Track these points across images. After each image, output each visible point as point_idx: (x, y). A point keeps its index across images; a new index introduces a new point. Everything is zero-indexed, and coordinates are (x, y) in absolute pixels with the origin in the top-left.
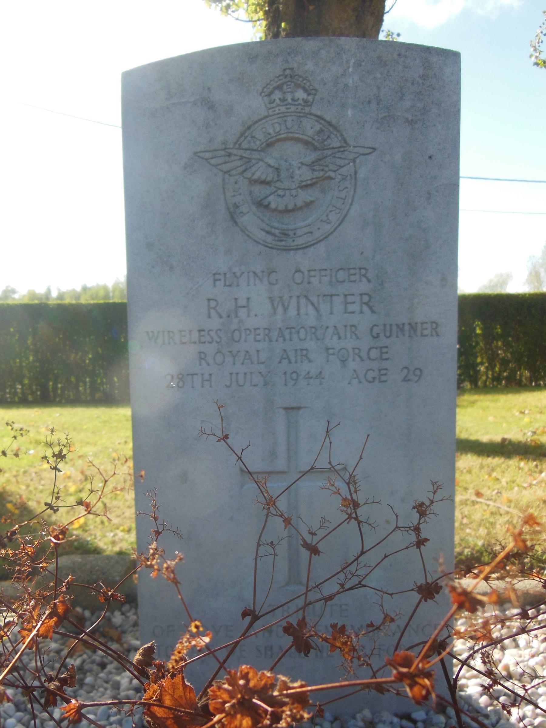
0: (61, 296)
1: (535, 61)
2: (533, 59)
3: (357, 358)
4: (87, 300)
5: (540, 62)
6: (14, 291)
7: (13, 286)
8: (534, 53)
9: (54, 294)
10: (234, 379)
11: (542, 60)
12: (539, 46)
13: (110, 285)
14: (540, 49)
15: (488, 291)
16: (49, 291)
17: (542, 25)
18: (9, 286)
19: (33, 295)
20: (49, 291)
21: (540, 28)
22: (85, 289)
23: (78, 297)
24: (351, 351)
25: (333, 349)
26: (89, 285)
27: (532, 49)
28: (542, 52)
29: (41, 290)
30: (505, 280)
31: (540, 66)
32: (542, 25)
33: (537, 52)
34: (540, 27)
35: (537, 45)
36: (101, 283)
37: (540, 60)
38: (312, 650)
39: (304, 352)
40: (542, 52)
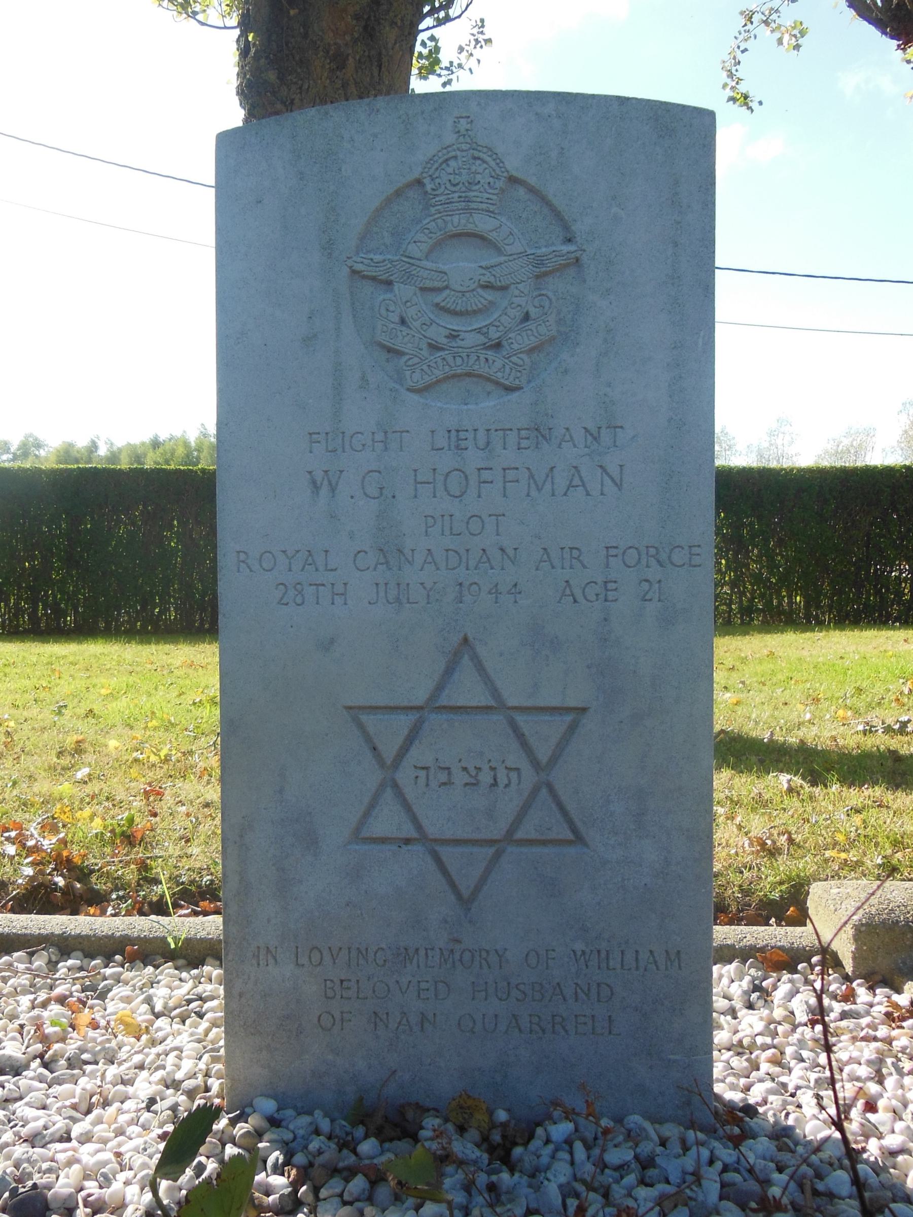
0: (114, 457)
1: (732, 94)
2: (728, 93)
3: (653, 562)
4: (158, 464)
5: (739, 97)
6: (39, 446)
7: (41, 437)
8: (729, 81)
9: (103, 451)
10: (382, 594)
11: (742, 94)
12: (737, 71)
13: (192, 438)
14: (738, 75)
15: (825, 463)
16: (94, 446)
17: (737, 35)
18: (31, 435)
19: (67, 453)
20: (94, 446)
21: (734, 40)
22: (156, 444)
23: (138, 458)
24: (643, 551)
25: (616, 547)
26: (163, 436)
27: (725, 74)
28: (741, 80)
29: (82, 442)
30: (859, 450)
31: (738, 103)
32: (737, 35)
33: (733, 81)
34: (736, 38)
35: (734, 69)
36: (178, 433)
37: (738, 93)
38: (138, 1093)
39: (575, 553)
40: (741, 80)
